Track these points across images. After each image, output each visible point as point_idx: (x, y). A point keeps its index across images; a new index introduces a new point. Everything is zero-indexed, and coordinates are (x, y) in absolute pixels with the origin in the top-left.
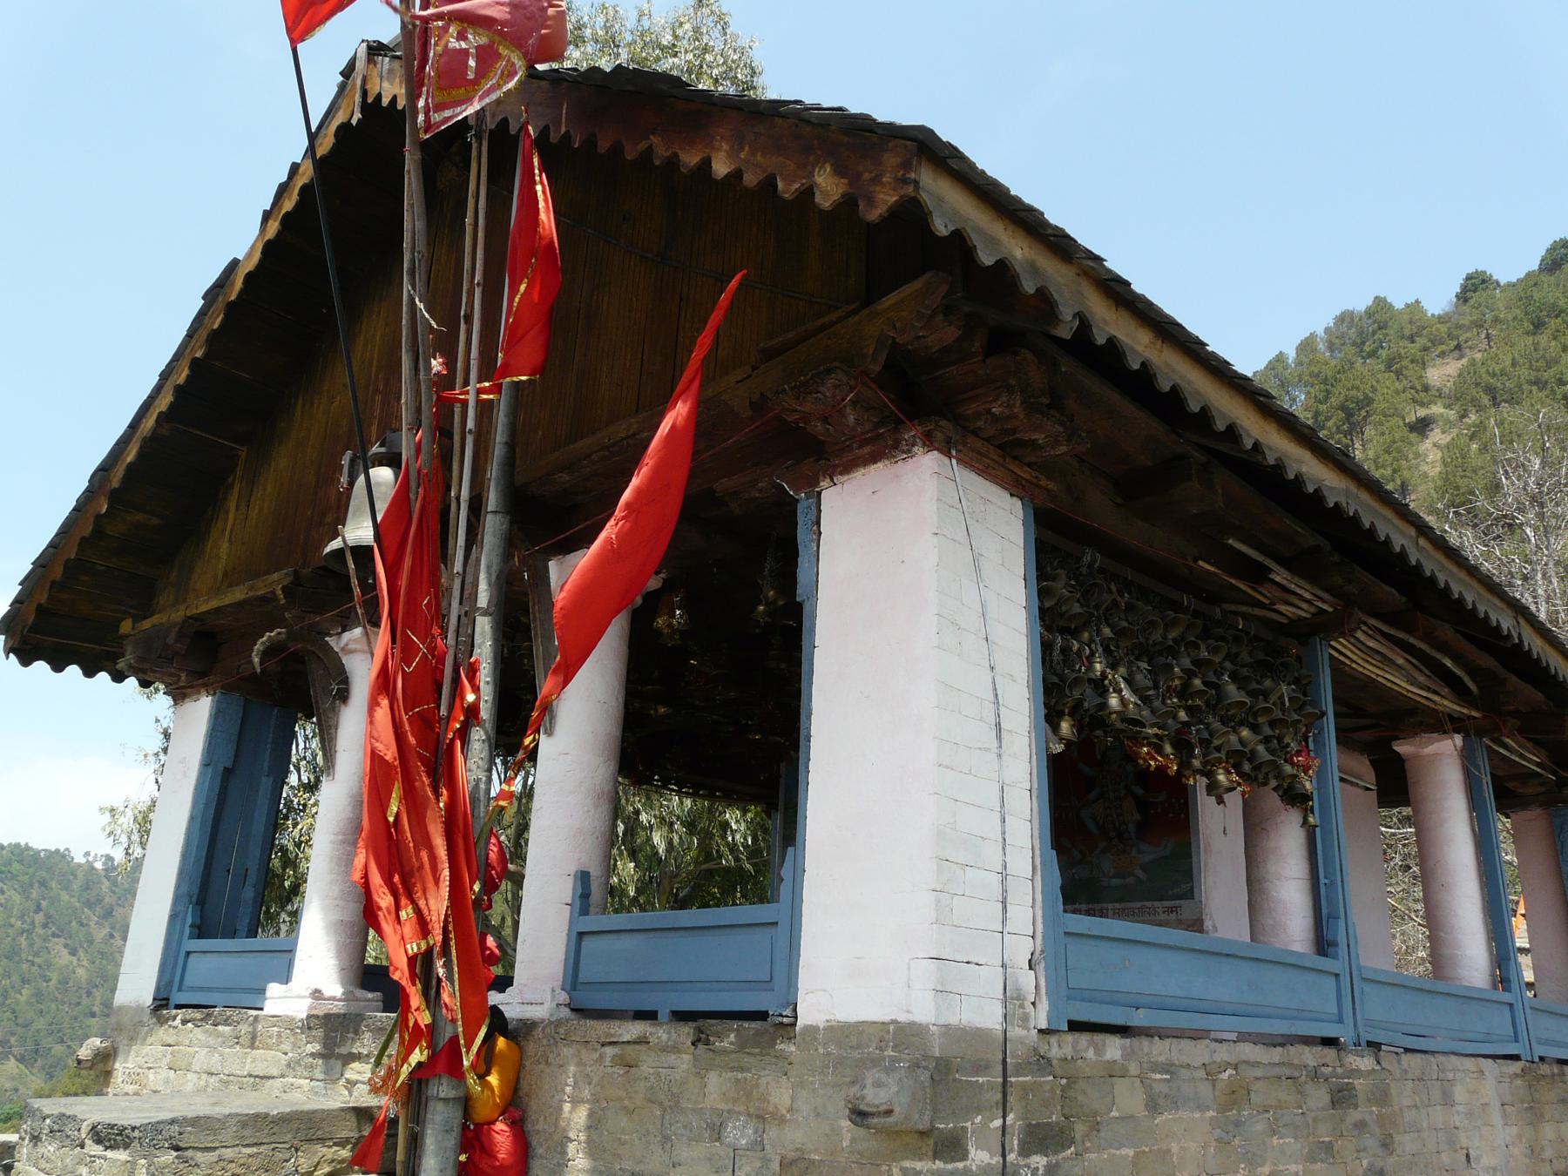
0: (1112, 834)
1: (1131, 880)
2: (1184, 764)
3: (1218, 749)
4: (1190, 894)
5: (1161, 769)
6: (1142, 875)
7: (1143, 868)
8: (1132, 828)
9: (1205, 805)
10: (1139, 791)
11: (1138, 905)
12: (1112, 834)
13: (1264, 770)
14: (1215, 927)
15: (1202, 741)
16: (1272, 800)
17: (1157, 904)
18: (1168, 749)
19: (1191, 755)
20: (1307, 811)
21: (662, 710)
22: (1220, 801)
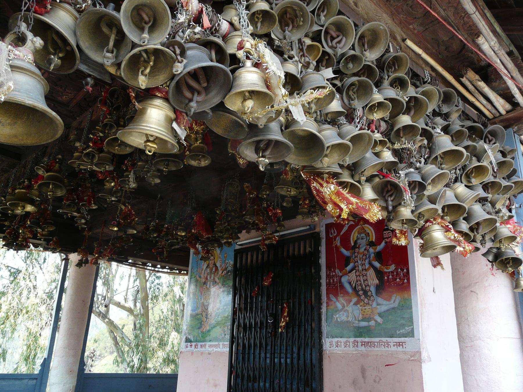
0: (361, 293)
1: (372, 323)
2: (392, 213)
3: (433, 200)
4: (411, 334)
5: (357, 218)
6: (379, 320)
7: (380, 315)
8: (373, 289)
9: (421, 266)
10: (377, 264)
11: (377, 340)
12: (361, 293)
13: (482, 231)
14: (429, 357)
15: (412, 185)
16: (481, 264)
17: (389, 339)
18: (369, 193)
19: (399, 203)
20: (514, 277)
21: (116, 229)
22: (436, 263)
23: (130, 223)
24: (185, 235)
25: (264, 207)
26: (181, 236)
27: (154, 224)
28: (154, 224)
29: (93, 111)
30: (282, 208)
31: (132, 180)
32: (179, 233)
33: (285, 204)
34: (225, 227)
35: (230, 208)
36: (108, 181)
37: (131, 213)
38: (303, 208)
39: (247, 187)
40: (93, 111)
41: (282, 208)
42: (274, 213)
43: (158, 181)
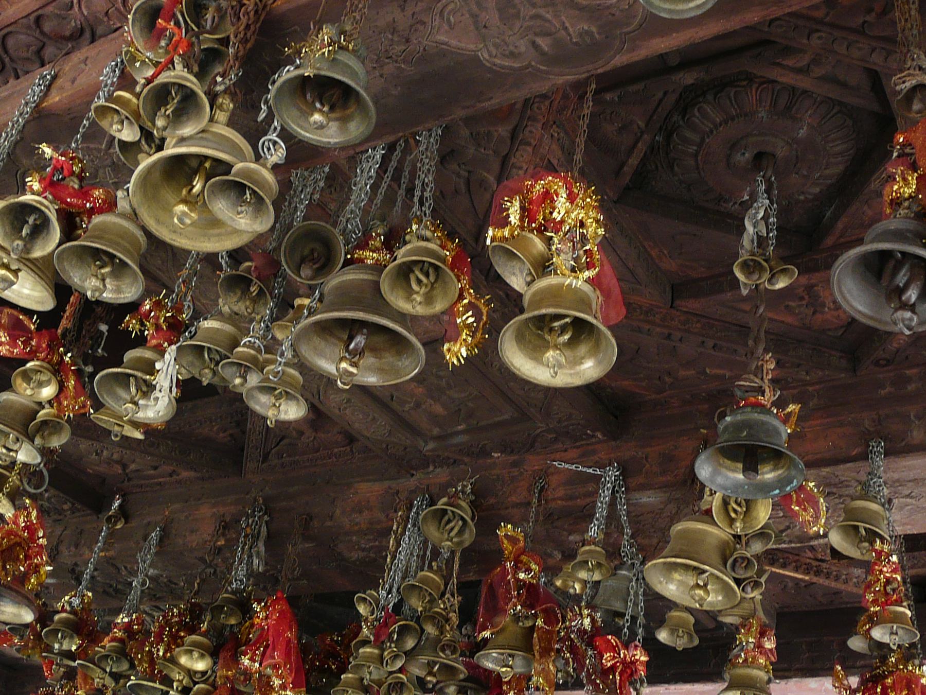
23: (23, 579)
24: (204, 673)
25: (582, 632)
26: (190, 673)
27: (76, 601)
28: (76, 601)
29: (54, 78)
30: (651, 644)
31: (166, 385)
32: (183, 660)
33: (663, 636)
34: (391, 673)
35: (417, 604)
36: (27, 377)
37: (33, 537)
38: (754, 664)
39: (513, 540)
40: (54, 78)
41: (651, 644)
42: (623, 662)
43: (292, 411)
